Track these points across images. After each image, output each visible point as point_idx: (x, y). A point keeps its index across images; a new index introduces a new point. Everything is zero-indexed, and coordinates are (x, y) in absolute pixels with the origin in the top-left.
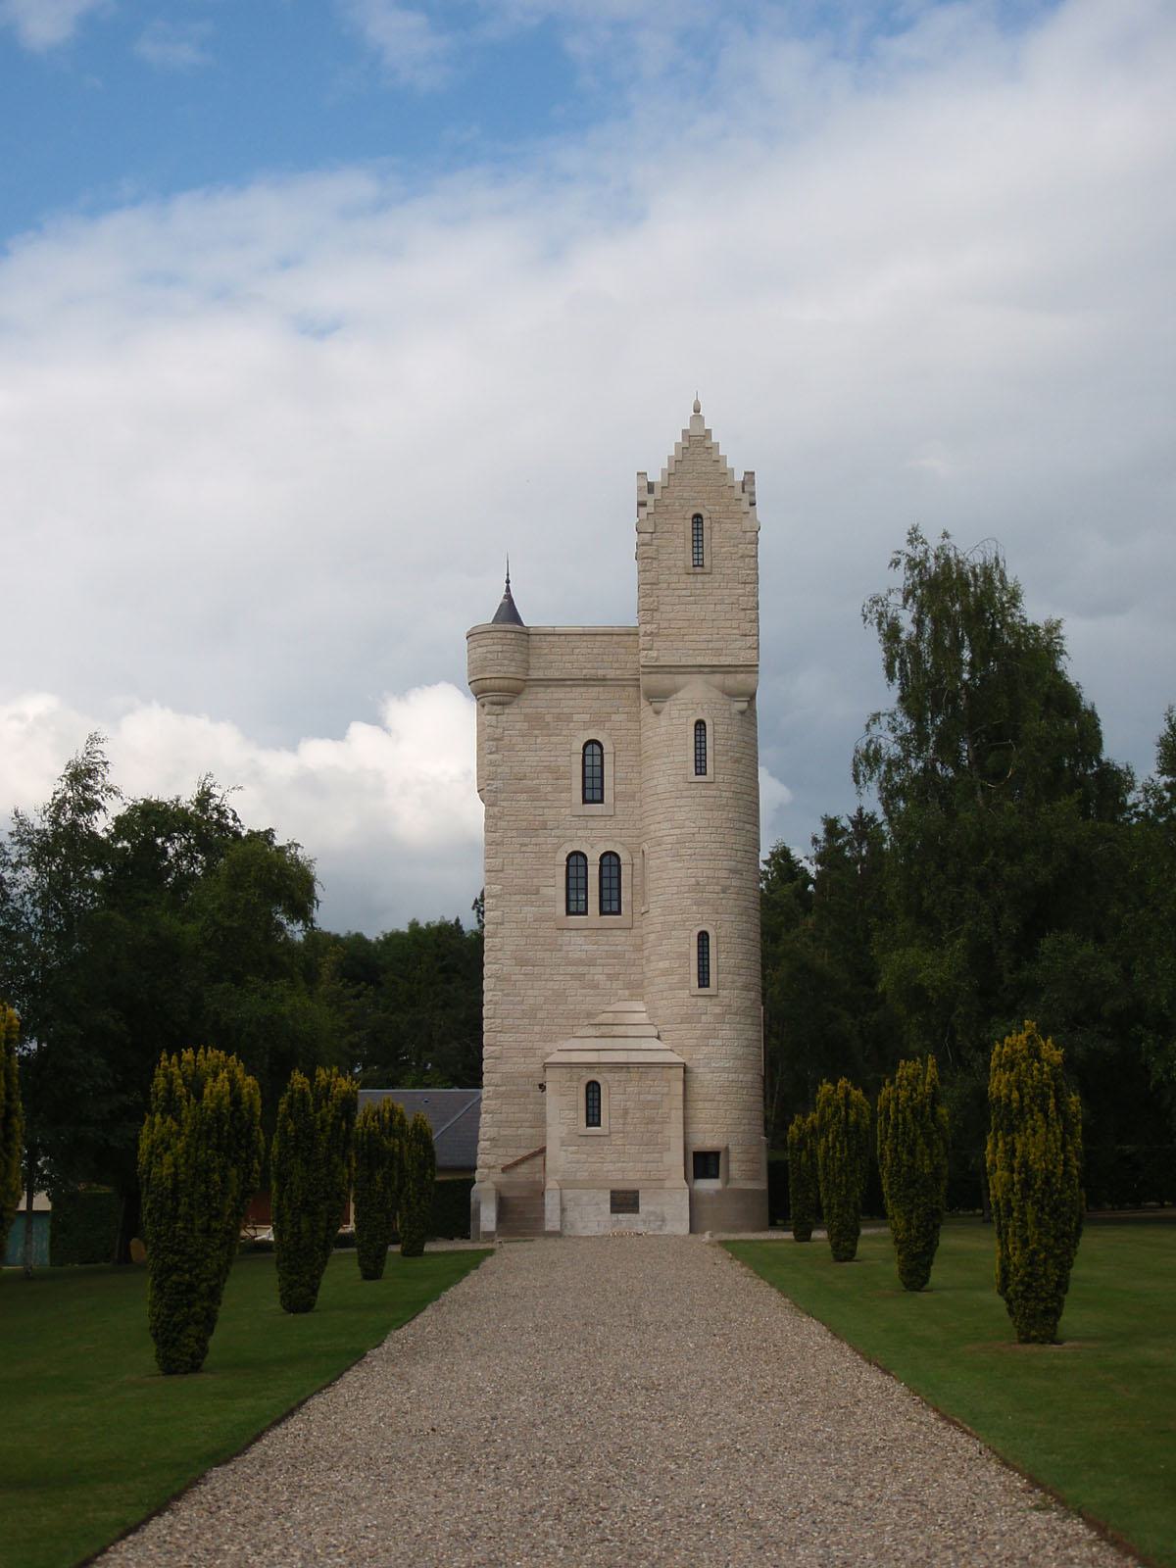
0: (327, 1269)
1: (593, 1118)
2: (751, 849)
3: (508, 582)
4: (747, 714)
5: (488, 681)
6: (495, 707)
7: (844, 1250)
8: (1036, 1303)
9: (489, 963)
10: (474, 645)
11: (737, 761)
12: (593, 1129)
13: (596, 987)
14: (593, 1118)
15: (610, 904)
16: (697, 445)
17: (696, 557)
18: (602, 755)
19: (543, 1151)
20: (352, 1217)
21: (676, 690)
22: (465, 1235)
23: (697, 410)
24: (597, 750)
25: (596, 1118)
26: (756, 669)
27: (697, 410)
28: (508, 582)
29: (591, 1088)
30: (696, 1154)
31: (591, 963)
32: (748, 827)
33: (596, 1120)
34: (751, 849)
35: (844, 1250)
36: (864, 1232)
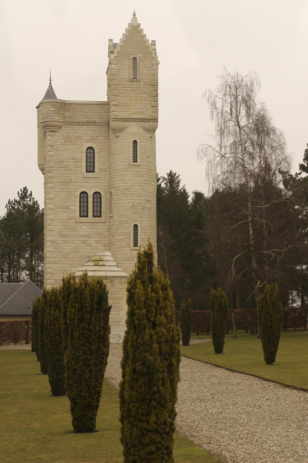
4: (153, 138)
15: (98, 214)
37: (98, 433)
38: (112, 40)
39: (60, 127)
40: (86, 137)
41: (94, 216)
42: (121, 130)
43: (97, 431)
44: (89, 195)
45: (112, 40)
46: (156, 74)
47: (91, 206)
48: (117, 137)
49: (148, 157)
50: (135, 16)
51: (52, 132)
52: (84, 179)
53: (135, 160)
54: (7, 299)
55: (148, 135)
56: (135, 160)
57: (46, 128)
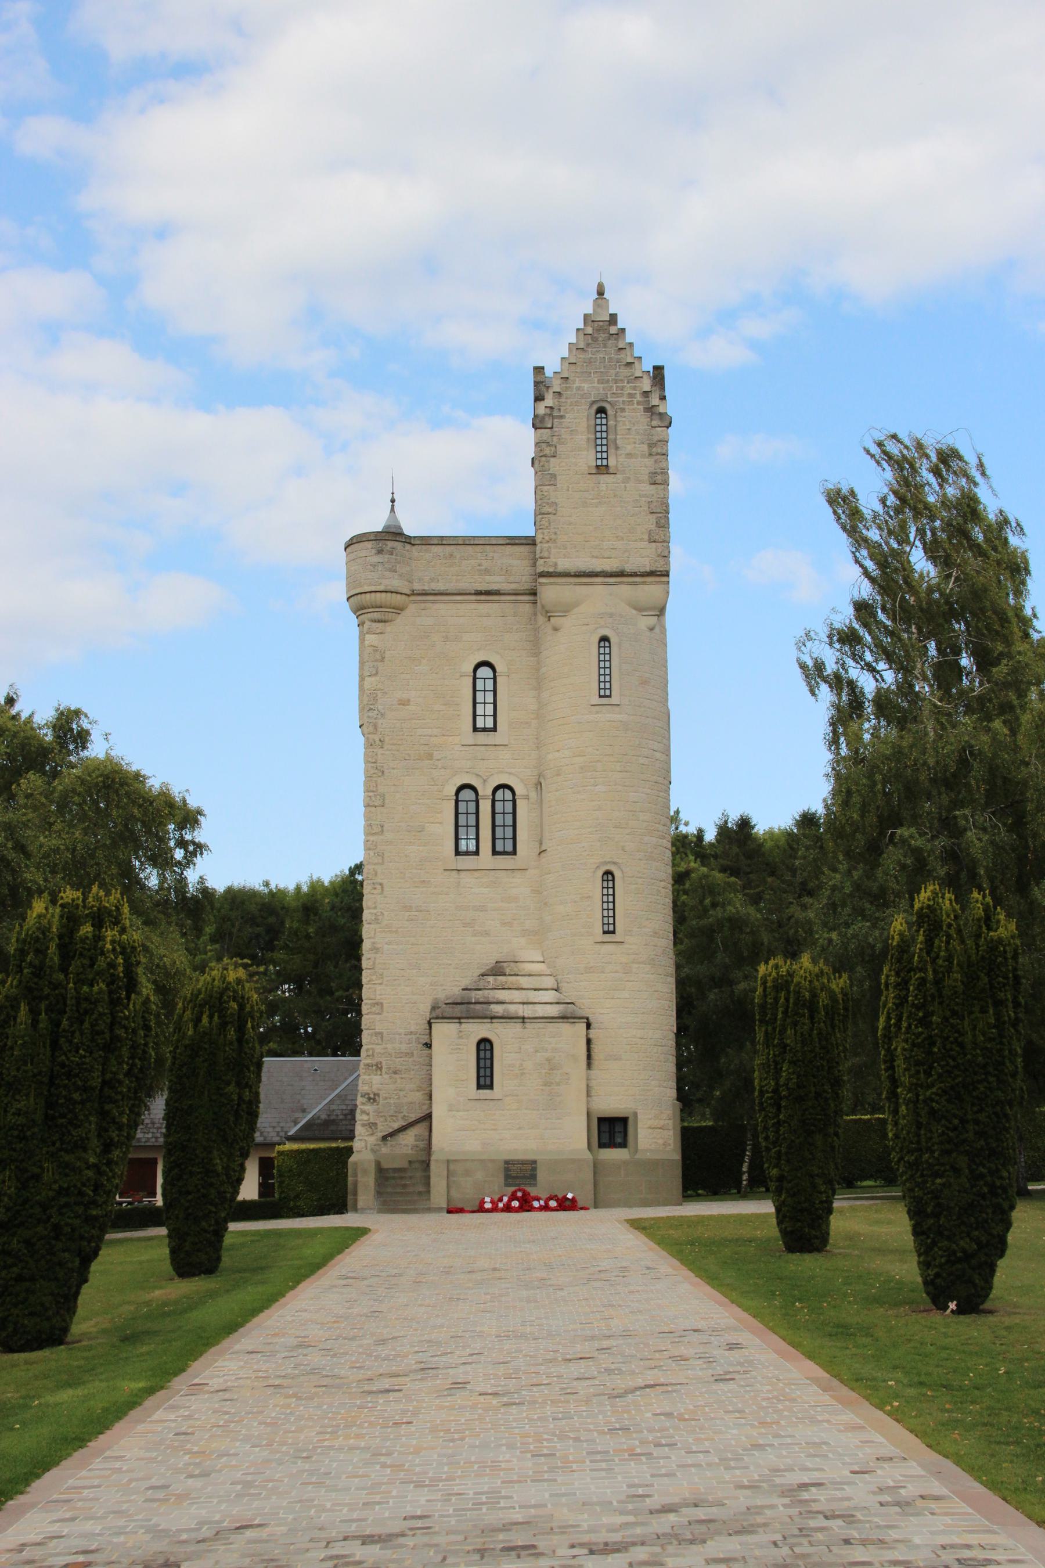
0: (101, 1253)
1: (485, 1079)
2: (661, 780)
3: (393, 501)
4: (657, 630)
5: (368, 595)
6: (374, 624)
7: (804, 1230)
8: (959, 1271)
9: (369, 908)
10: (352, 556)
11: (519, 1557)
12: (485, 1093)
13: (487, 934)
14: (485, 1079)
15: (505, 846)
16: (602, 331)
17: (599, 455)
18: (514, 801)
19: (428, 1117)
20: (159, 1190)
21: (576, 604)
22: (341, 1207)
23: (601, 293)
24: (508, 795)
25: (488, 1080)
26: (664, 579)
27: (601, 293)
28: (393, 501)
29: (482, 1047)
30: (601, 1120)
31: (482, 909)
32: (658, 755)
33: (488, 1082)
34: (661, 780)
35: (804, 1230)
36: (836, 1205)
37: (991, 1319)
38: (543, 368)
39: (399, 609)
40: (482, 631)
41: (495, 853)
42: (566, 610)
43: (990, 1312)
44: (517, 793)
45: (543, 368)
46: (664, 452)
47: (489, 822)
48: (556, 629)
49: (644, 682)
50: (603, 294)
51: (380, 621)
52: (467, 748)
53: (605, 694)
54: (346, 1079)
55: (645, 622)
56: (605, 694)
57: (370, 607)
